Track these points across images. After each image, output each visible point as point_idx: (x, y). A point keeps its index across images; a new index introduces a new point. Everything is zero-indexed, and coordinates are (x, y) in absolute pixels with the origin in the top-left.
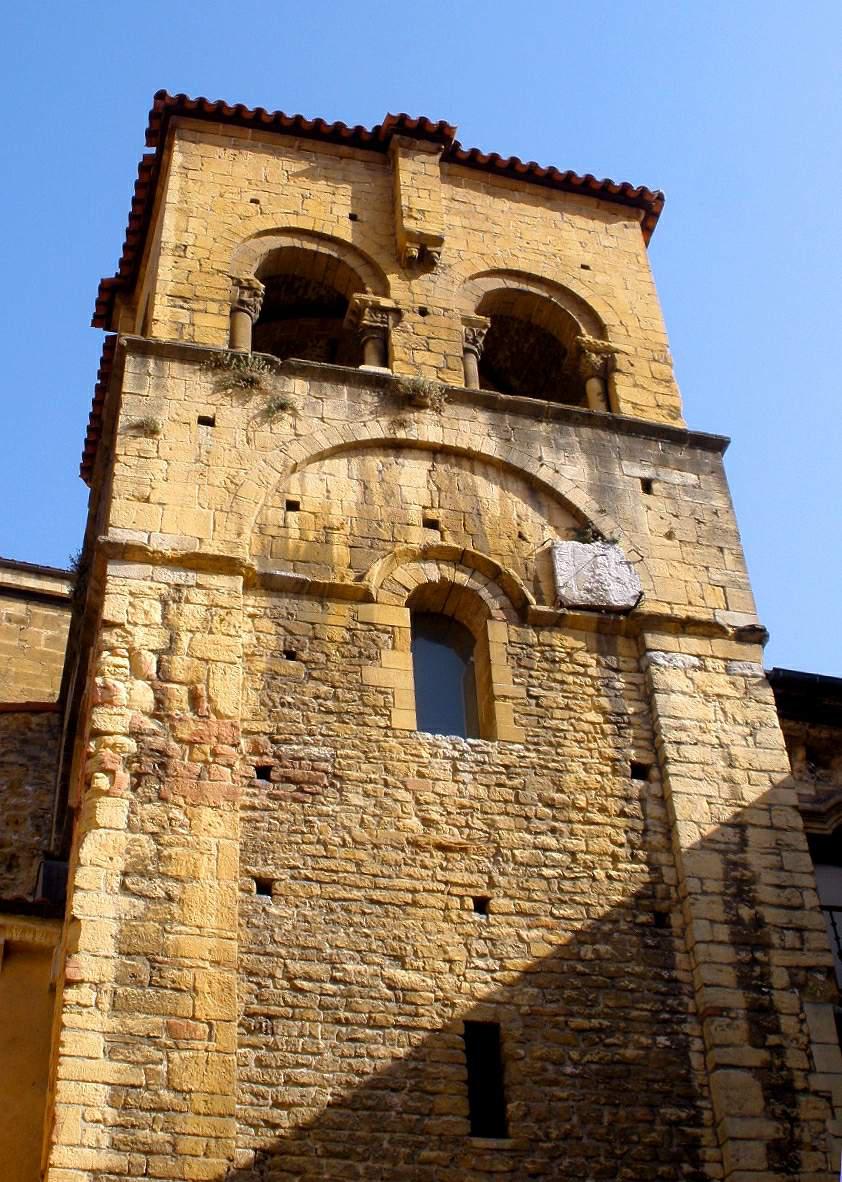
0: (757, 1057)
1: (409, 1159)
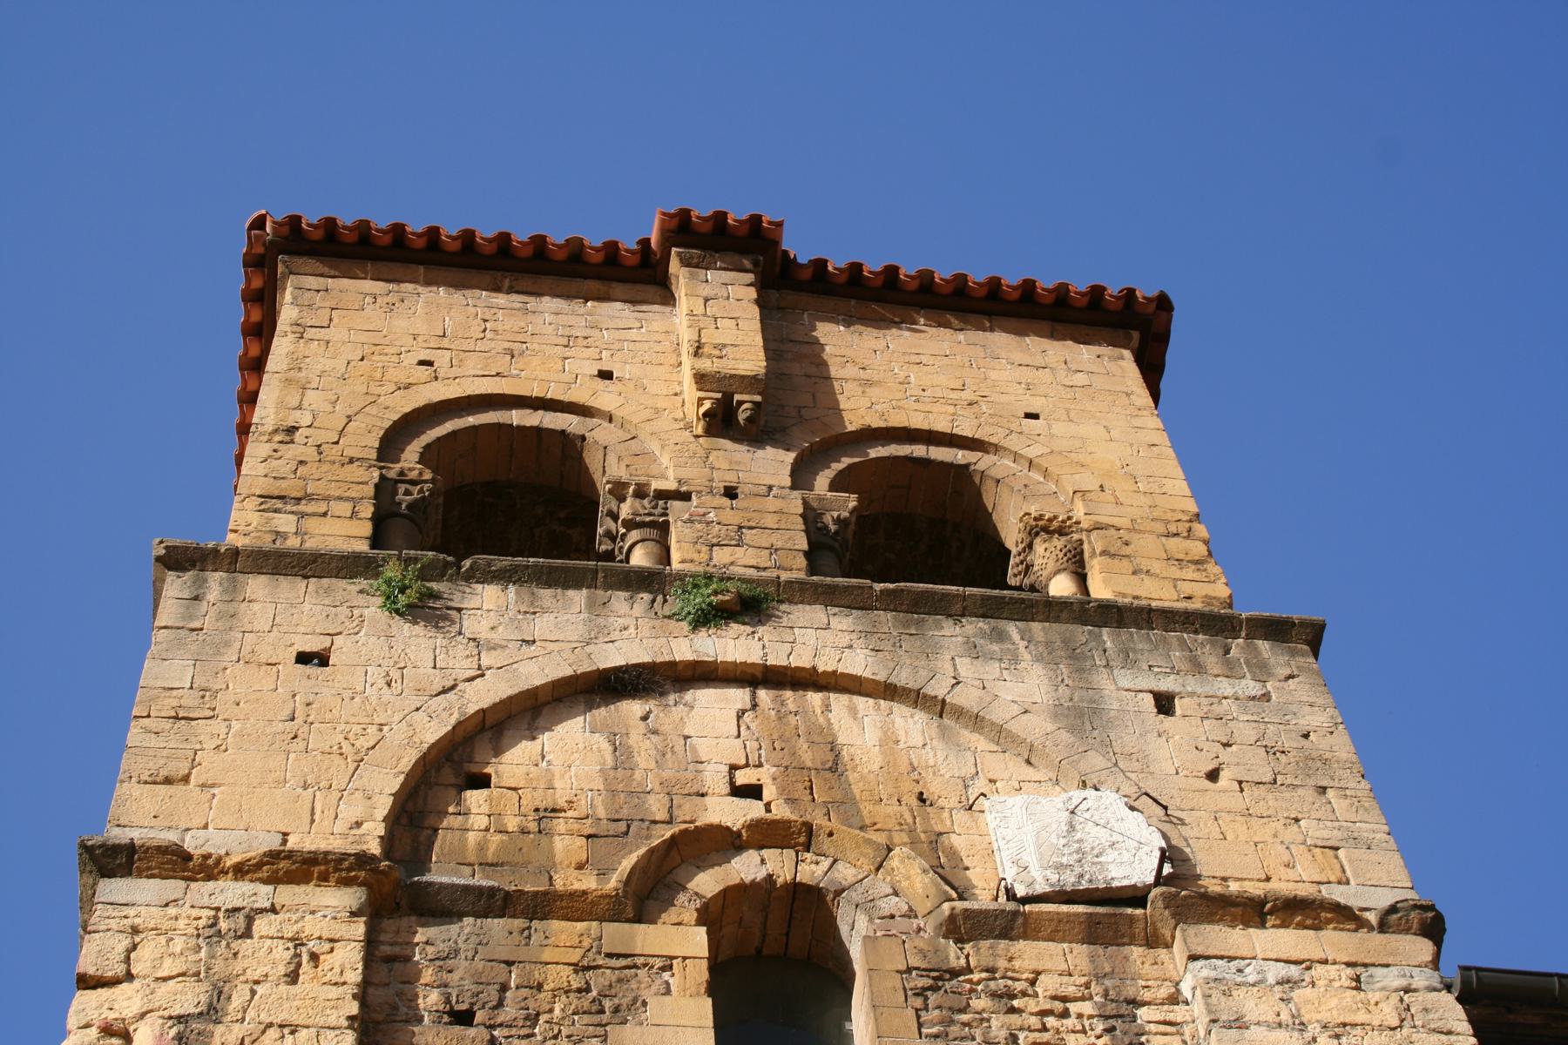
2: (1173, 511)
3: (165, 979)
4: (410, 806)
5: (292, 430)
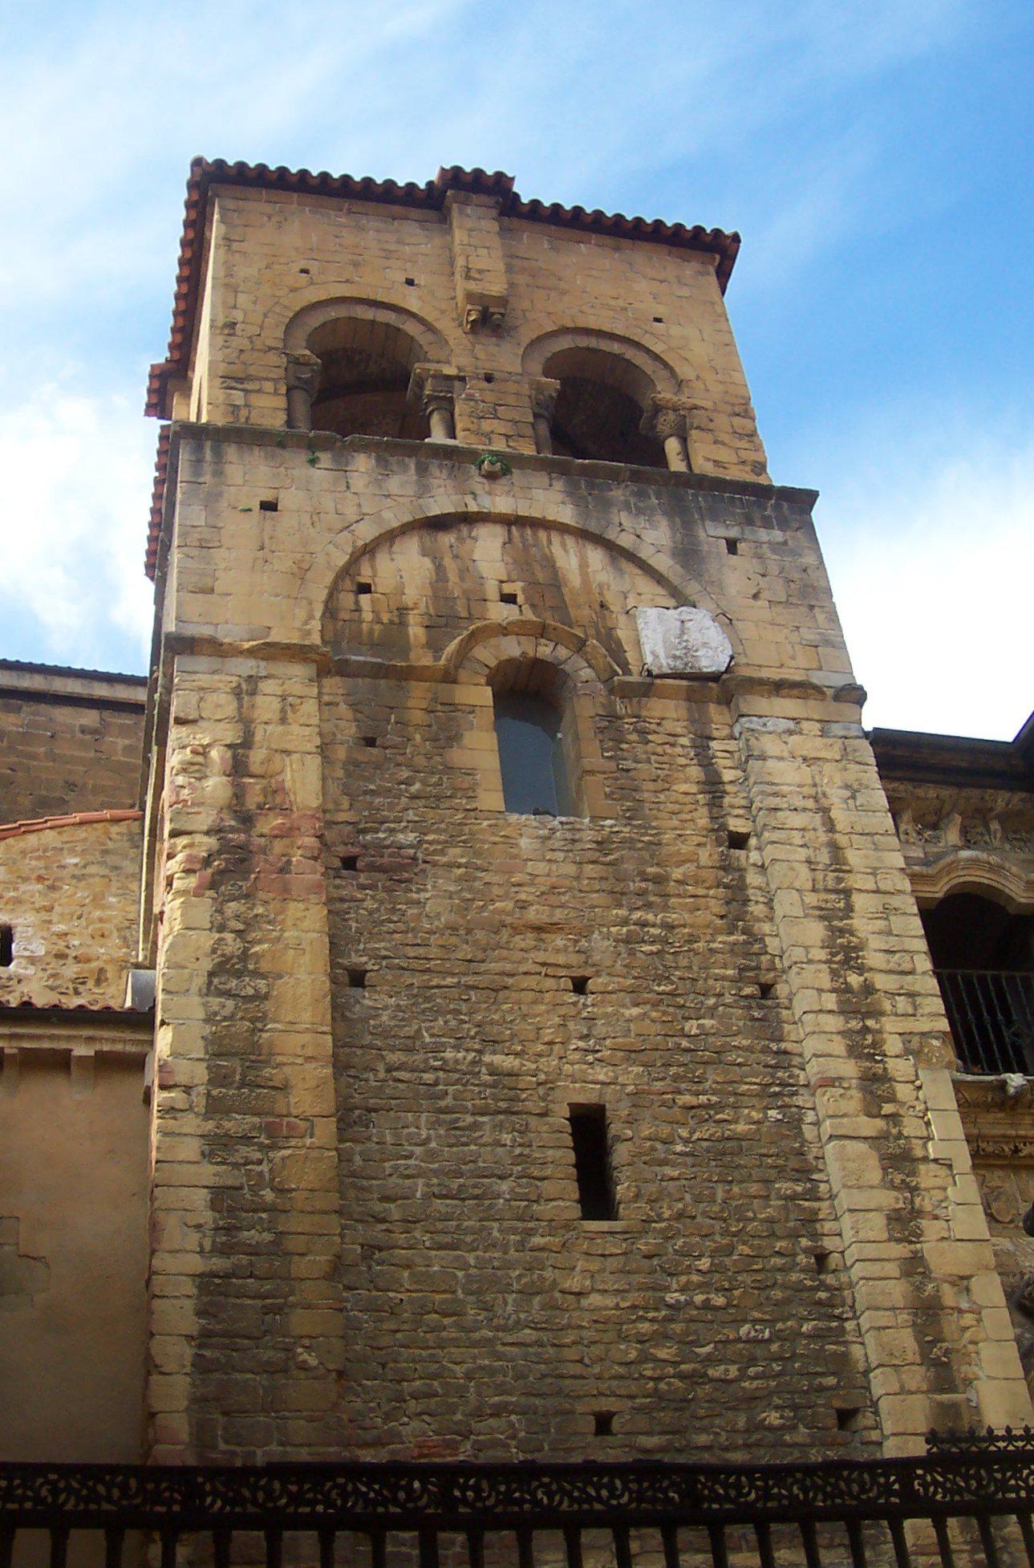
0: (871, 1126)
1: (521, 1246)
2: (737, 397)
3: (220, 720)
5: (233, 325)
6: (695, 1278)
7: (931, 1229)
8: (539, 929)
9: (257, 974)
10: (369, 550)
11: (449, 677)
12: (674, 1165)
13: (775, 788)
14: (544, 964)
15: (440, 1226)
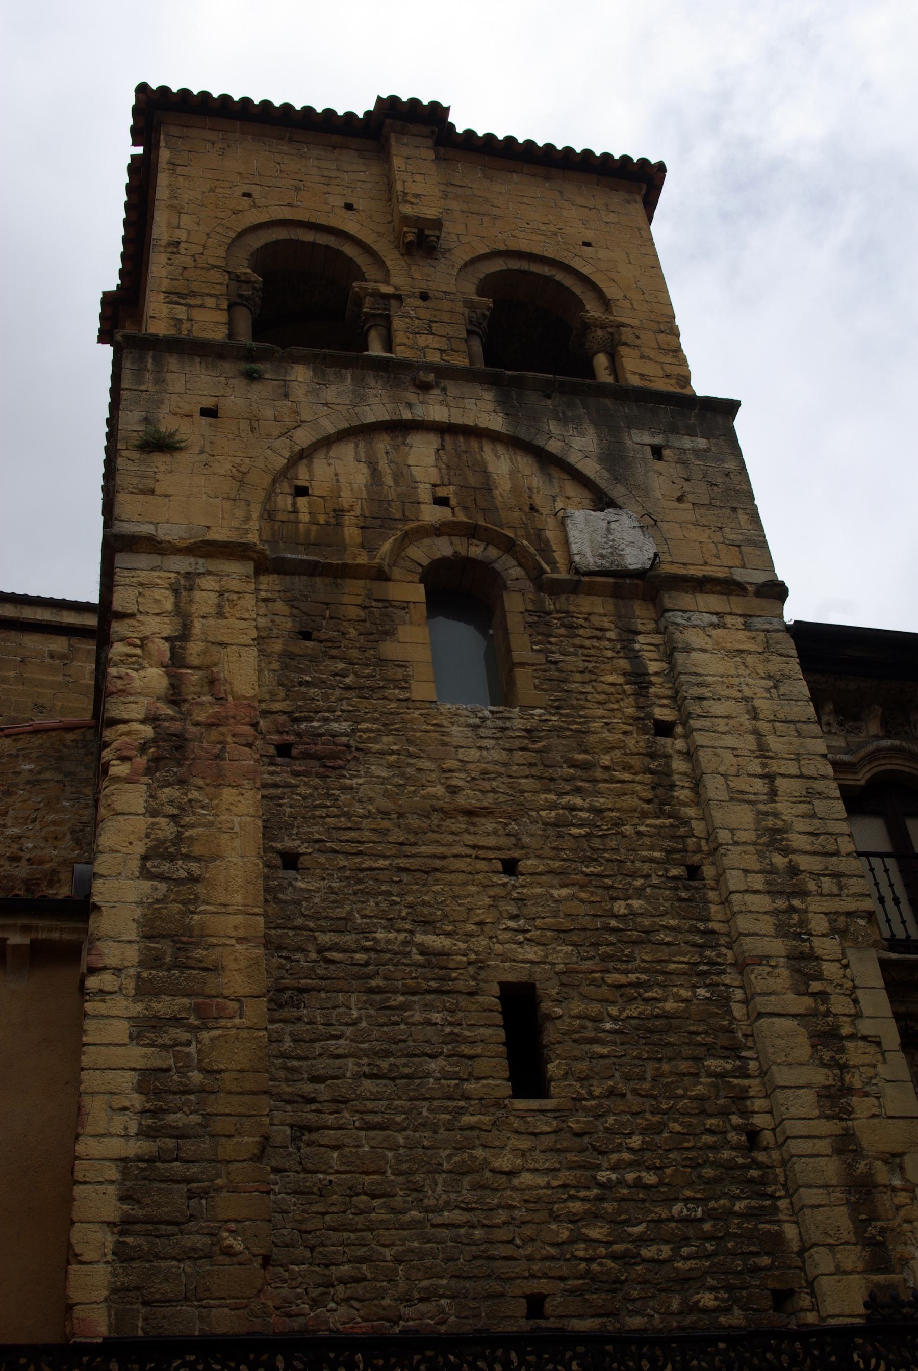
4: (268, 507)
6: (626, 1156)
7: (862, 1106)
8: (470, 813)
9: (187, 857)
10: (304, 455)
11: (381, 575)
12: (603, 1043)
13: (700, 679)
14: (474, 847)
15: (370, 1105)
